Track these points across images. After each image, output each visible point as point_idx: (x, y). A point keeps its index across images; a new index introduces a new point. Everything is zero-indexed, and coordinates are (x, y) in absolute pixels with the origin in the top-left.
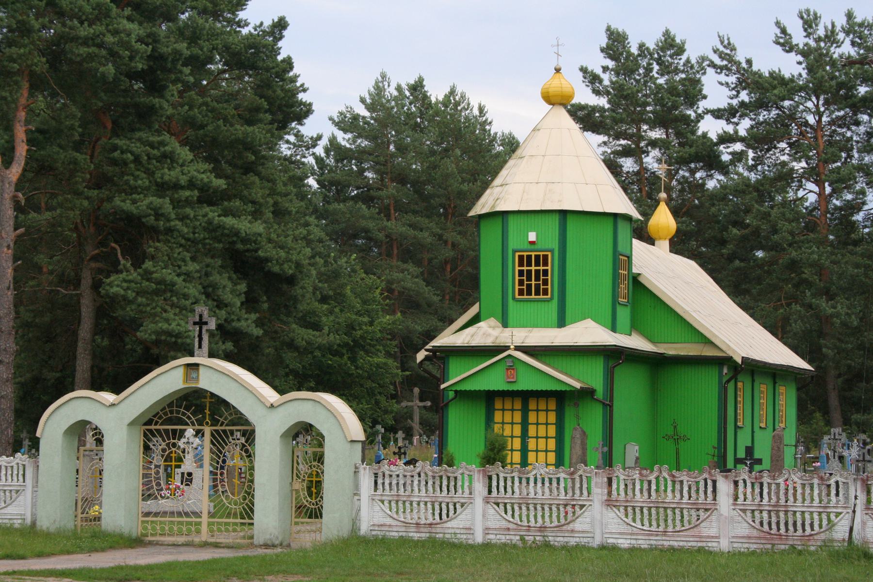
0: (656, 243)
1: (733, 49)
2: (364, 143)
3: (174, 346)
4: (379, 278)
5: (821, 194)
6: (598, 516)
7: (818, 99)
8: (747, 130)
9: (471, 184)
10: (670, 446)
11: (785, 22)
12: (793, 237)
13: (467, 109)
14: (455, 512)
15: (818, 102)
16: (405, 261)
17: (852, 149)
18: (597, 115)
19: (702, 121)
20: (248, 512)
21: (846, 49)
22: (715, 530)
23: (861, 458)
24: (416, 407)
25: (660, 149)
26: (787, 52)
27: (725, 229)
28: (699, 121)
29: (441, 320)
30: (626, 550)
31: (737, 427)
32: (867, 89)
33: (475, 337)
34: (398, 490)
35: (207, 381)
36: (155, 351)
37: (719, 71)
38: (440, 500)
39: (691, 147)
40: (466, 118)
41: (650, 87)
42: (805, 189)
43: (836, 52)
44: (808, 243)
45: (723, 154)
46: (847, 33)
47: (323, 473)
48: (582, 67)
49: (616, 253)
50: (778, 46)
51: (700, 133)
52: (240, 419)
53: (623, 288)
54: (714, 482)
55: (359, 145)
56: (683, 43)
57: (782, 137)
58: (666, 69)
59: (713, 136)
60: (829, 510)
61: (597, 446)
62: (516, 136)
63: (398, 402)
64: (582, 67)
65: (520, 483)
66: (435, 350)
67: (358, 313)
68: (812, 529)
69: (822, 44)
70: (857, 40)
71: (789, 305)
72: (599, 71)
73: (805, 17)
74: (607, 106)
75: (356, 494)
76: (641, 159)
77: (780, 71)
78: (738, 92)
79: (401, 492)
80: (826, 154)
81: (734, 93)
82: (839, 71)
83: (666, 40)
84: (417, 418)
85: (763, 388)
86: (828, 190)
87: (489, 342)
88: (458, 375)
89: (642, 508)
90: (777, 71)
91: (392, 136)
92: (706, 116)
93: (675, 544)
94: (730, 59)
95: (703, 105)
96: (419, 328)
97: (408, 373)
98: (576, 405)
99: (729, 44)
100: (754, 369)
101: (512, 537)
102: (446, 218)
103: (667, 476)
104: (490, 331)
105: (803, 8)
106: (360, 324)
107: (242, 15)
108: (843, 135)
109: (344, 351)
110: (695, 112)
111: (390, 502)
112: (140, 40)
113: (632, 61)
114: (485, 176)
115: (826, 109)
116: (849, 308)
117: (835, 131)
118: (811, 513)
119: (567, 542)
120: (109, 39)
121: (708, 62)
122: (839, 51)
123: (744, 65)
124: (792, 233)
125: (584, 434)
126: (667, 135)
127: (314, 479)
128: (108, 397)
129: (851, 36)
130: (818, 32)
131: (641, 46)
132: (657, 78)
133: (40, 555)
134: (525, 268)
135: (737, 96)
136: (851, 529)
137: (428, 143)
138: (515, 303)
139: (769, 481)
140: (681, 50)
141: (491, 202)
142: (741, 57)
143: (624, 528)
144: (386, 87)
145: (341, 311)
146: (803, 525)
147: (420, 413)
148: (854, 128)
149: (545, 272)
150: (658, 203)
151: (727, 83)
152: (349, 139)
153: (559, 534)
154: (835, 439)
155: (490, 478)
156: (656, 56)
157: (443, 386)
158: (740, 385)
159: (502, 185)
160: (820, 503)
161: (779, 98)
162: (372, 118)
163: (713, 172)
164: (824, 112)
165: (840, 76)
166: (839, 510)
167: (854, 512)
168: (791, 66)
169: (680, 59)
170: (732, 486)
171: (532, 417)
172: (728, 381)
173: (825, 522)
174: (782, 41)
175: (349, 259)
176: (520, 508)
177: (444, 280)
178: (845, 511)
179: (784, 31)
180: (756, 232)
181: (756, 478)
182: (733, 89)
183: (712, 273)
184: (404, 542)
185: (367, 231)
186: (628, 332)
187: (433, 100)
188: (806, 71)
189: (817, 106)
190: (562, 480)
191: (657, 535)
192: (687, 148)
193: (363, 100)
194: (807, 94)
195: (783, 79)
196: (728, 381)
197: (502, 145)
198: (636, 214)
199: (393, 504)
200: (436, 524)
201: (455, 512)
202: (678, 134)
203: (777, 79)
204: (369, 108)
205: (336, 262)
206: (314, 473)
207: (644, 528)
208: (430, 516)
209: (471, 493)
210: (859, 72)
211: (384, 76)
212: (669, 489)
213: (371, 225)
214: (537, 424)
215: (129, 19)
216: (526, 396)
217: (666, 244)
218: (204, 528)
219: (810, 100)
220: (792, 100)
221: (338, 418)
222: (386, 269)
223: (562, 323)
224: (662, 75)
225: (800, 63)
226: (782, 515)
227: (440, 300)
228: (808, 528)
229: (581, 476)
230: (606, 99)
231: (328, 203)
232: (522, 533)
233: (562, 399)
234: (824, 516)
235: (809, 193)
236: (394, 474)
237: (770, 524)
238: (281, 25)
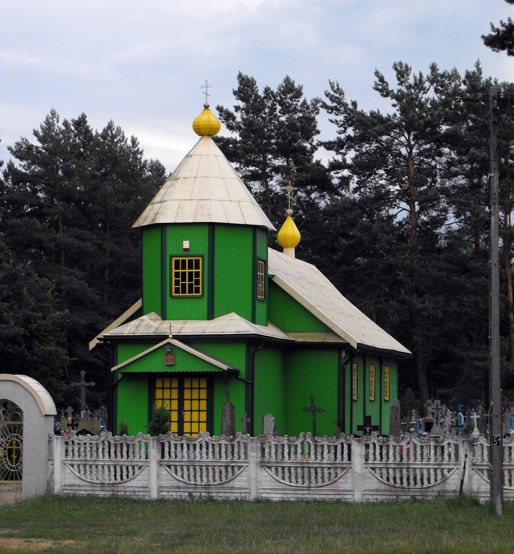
0: (284, 250)
1: (342, 93)
2: (37, 169)
4: (51, 280)
5: (412, 211)
6: (253, 475)
7: (409, 135)
8: (353, 159)
9: (125, 203)
11: (382, 72)
12: (390, 246)
13: (122, 141)
14: (233, 475)
15: (409, 137)
16: (71, 267)
17: (436, 175)
18: (231, 146)
19: (316, 152)
22: (350, 485)
23: (455, 424)
24: (82, 387)
25: (282, 175)
26: (385, 96)
27: (336, 239)
28: (314, 152)
29: (101, 315)
30: (276, 502)
31: (352, 401)
32: (447, 127)
33: (139, 328)
34: (85, 455)
37: (330, 111)
38: (121, 463)
39: (307, 172)
40: (121, 148)
41: (274, 123)
42: (399, 207)
43: (423, 97)
44: (402, 251)
45: (333, 178)
46: (432, 82)
47: (22, 441)
48: (219, 106)
49: (255, 259)
50: (378, 92)
51: (314, 161)
54: (349, 446)
55: (33, 170)
56: (301, 88)
57: (381, 165)
58: (286, 109)
59: (325, 164)
60: (443, 467)
61: (241, 417)
62: (162, 163)
63: (68, 383)
64: (219, 106)
65: (188, 448)
66: (106, 339)
67: (33, 310)
68: (429, 483)
69: (413, 91)
70: (439, 87)
71: (387, 301)
72: (232, 110)
73: (399, 68)
74: (239, 139)
75: (50, 459)
76: (267, 183)
77: (379, 112)
78: (346, 129)
79: (88, 457)
80: (416, 179)
81: (342, 129)
82: (426, 112)
83: (286, 85)
84: (83, 396)
85: (372, 368)
86: (417, 208)
87: (151, 332)
88: (125, 360)
89: (290, 468)
90: (377, 112)
91: (60, 163)
92: (319, 148)
93: (318, 497)
94: (339, 101)
95: (316, 139)
96: (83, 322)
97: (74, 359)
98: (226, 384)
99: (338, 89)
101: (182, 494)
102: (105, 231)
103: (310, 442)
104: (152, 323)
105: (397, 61)
106: (35, 319)
108: (429, 164)
109: (22, 341)
110: (311, 144)
111: (79, 465)
113: (259, 102)
114: (137, 196)
115: (416, 143)
116: (435, 304)
117: (423, 160)
118: (429, 469)
119: (228, 497)
121: (321, 104)
122: (425, 96)
123: (350, 106)
124: (389, 243)
125: (232, 407)
126: (287, 162)
127: (14, 447)
129: (435, 84)
130: (409, 81)
131: (267, 90)
132: (280, 116)
134: (180, 271)
135: (344, 132)
136: (462, 482)
137: (90, 168)
138: (172, 300)
139: (394, 444)
140: (298, 94)
141: (151, 216)
142: (348, 100)
143: (274, 485)
144: (55, 122)
145: (20, 308)
146: (422, 479)
147: (86, 392)
148: (437, 158)
149: (197, 274)
150: (285, 219)
151: (337, 121)
152: (25, 165)
153: (221, 491)
154: (437, 409)
155: (163, 445)
156: (279, 98)
157: (113, 369)
158: (355, 366)
159: (160, 202)
160: (394, 461)
161: (379, 133)
162: (44, 148)
163: (325, 193)
164: (414, 145)
165: (427, 116)
166: (451, 467)
167: (465, 468)
168: (388, 108)
169: (298, 101)
170: (364, 448)
171: (187, 394)
172: (346, 363)
173: (439, 477)
174: (380, 87)
175: (25, 264)
176: (188, 470)
177: (103, 282)
178: (455, 467)
179: (382, 79)
180: (360, 243)
181: (384, 442)
182: (341, 126)
184: (91, 499)
186: (265, 324)
187: (94, 133)
188: (399, 112)
189: (408, 141)
190: (223, 446)
191: (302, 490)
192: (304, 174)
193: (36, 133)
194: (401, 130)
195: (381, 118)
196: (346, 363)
197: (150, 171)
198: (270, 226)
199: (82, 468)
200: (118, 484)
201: (233, 475)
202: (296, 163)
203: (376, 117)
204: (41, 140)
205: (14, 267)
206: (14, 442)
207: (292, 484)
208: (113, 478)
209: (147, 458)
210: (442, 113)
211: (53, 113)
212: (312, 452)
213: (43, 236)
214: (191, 400)
216: (181, 378)
217: (292, 251)
219: (403, 135)
220: (389, 135)
222: (56, 273)
223: (211, 316)
224: (284, 114)
225: (394, 106)
226: (404, 471)
227: (101, 299)
228: (425, 481)
229: (239, 442)
230: (239, 133)
231: (7, 218)
232: (190, 490)
233: (213, 379)
234: (439, 472)
235: (400, 212)
236: (82, 442)
237: (395, 479)
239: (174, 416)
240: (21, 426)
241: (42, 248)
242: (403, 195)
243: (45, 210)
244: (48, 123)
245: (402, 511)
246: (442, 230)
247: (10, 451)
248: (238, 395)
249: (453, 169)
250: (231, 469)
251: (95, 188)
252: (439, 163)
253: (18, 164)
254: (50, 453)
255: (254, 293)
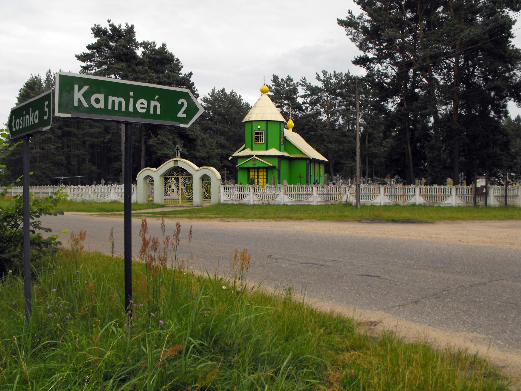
2: (210, 105)
3: (167, 158)
5: (328, 117)
10: (299, 179)
11: (318, 73)
20: (192, 197)
21: (334, 80)
35: (180, 165)
36: (161, 159)
43: (331, 81)
49: (280, 131)
52: (188, 174)
53: (282, 140)
58: (288, 85)
59: (301, 103)
66: (234, 157)
72: (271, 86)
75: (219, 192)
87: (248, 154)
88: (240, 163)
94: (305, 83)
95: (298, 95)
100: (315, 161)
107: (180, 72)
112: (156, 78)
120: (148, 78)
128: (155, 169)
131: (282, 79)
133: (140, 209)
140: (292, 80)
142: (308, 82)
143: (289, 200)
168: (320, 85)
171: (260, 174)
179: (318, 76)
180: (312, 127)
183: (302, 137)
184: (232, 205)
185: (211, 128)
193: (209, 94)
198: (285, 121)
202: (291, 102)
203: (317, 88)
204: (211, 96)
211: (214, 88)
213: (212, 126)
215: (153, 73)
216: (258, 168)
218: (180, 202)
221: (214, 173)
223: (267, 149)
233: (267, 169)
238: (191, 74)
239: (256, 181)
240: (210, 182)
241: (211, 130)
242: (325, 112)
243: (212, 118)
244: (213, 91)
245: (329, 207)
246: (338, 123)
247: (207, 190)
248: (276, 173)
249: (341, 104)
250: (276, 195)
251: (228, 111)
252: (337, 102)
253: (204, 104)
254: (220, 191)
255: (280, 142)
